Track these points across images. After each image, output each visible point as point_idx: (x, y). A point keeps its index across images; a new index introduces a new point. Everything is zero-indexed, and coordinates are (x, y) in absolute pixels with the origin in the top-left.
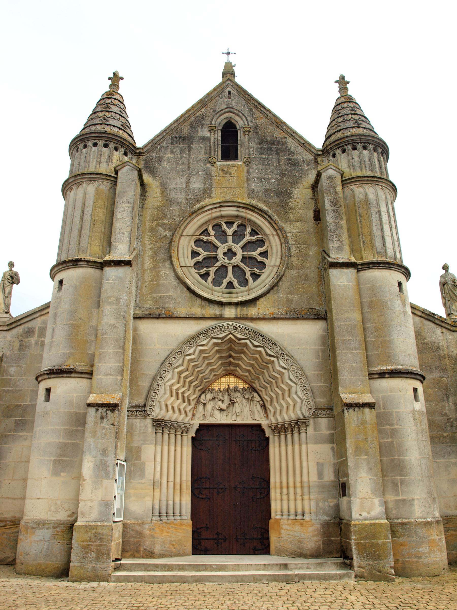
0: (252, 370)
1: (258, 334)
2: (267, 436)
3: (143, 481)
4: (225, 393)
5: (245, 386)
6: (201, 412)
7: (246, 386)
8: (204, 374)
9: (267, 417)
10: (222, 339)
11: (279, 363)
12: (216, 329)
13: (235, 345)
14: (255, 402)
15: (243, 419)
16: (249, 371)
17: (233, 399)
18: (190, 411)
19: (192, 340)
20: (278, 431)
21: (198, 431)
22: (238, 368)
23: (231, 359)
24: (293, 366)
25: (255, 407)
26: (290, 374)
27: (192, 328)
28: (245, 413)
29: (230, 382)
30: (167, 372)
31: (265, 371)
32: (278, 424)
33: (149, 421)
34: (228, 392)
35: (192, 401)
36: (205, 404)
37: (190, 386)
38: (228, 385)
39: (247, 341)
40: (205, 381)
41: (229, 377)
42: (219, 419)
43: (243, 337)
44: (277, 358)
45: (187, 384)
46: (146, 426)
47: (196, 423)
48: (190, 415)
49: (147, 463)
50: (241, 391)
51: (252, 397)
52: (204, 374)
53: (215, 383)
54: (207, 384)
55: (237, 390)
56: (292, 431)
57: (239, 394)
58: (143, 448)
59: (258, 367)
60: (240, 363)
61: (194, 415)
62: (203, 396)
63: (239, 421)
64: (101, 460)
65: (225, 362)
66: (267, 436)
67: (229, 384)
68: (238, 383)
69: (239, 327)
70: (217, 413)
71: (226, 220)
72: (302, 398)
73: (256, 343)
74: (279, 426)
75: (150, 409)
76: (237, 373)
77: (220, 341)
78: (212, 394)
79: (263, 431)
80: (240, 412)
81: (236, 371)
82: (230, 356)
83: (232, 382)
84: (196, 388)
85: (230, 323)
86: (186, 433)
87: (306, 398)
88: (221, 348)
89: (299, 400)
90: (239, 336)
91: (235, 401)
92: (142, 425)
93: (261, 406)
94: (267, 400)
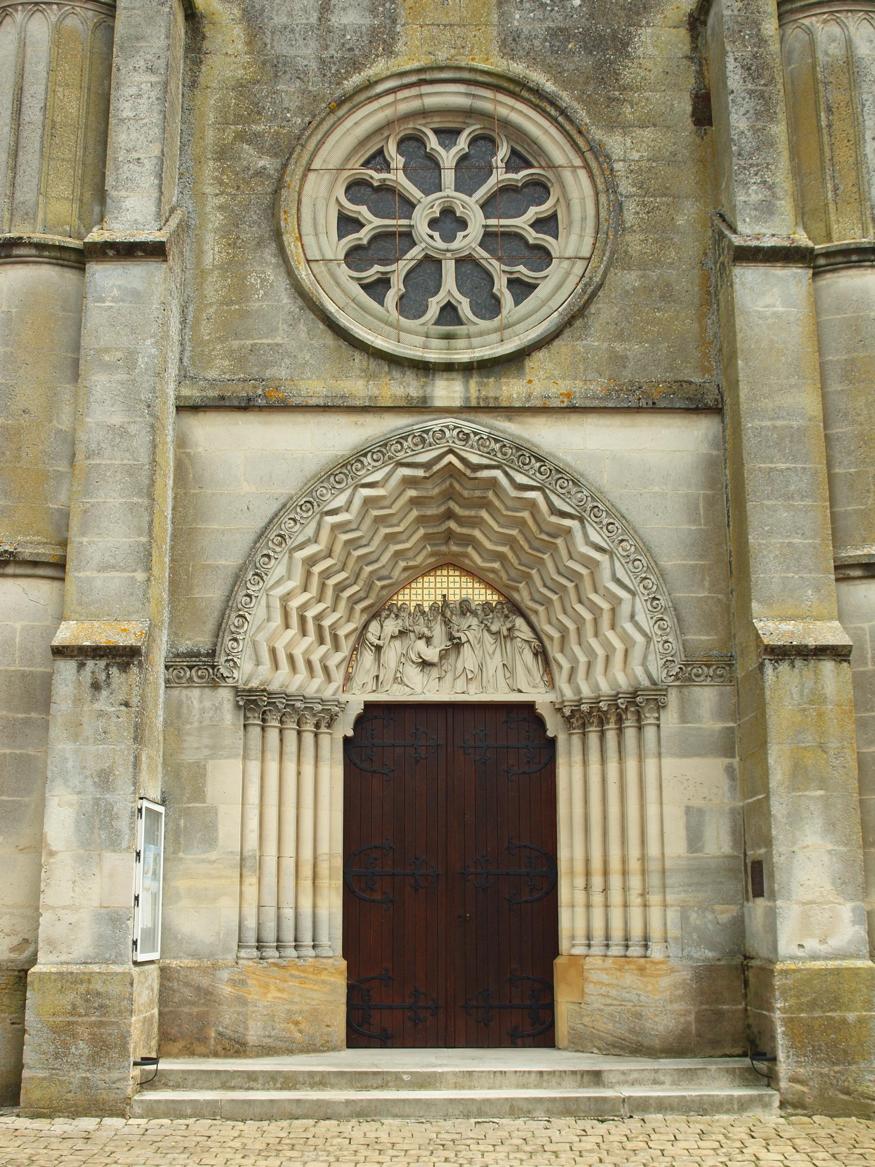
0: (510, 555)
1: (526, 454)
2: (550, 734)
3: (213, 855)
4: (435, 618)
5: (489, 598)
6: (368, 671)
7: (493, 598)
8: (375, 566)
9: (551, 684)
10: (427, 466)
11: (586, 535)
12: (410, 439)
13: (461, 485)
14: (518, 643)
15: (483, 689)
16: (500, 557)
17: (457, 635)
18: (338, 666)
19: (343, 470)
20: (580, 722)
21: (360, 721)
22: (470, 550)
23: (452, 525)
24: (624, 544)
25: (518, 657)
26: (617, 564)
27: (342, 435)
28: (491, 672)
29: (448, 588)
30: (273, 561)
31: (545, 557)
32: (580, 702)
33: (225, 695)
34: (443, 615)
35: (342, 640)
36: (379, 648)
37: (337, 599)
38: (444, 596)
39: (498, 474)
40: (379, 584)
41: (445, 572)
42: (418, 689)
43: (485, 461)
44: (581, 520)
45: (329, 592)
46: (217, 709)
47: (356, 701)
48: (338, 677)
49: (222, 809)
50: (479, 612)
51: (509, 630)
52: (375, 566)
53: (407, 591)
54: (384, 592)
55: (468, 610)
56: (620, 720)
57: (474, 622)
58: (209, 767)
59: (526, 547)
60: (477, 533)
61: (348, 678)
62: (374, 627)
63: (474, 695)
64: (97, 802)
65: (435, 530)
66: (550, 734)
67: (445, 592)
68: (470, 591)
69: (476, 434)
70: (413, 673)
71: (438, 122)
72: (648, 631)
73: (521, 479)
74: (585, 708)
75: (227, 661)
76: (467, 561)
77: (420, 473)
78: (400, 621)
79: (540, 722)
80: (476, 670)
81: (466, 555)
82: (450, 515)
83: (454, 587)
84: (356, 603)
85: (450, 421)
86: (329, 726)
87: (659, 632)
88: (424, 494)
89: (639, 638)
90: (474, 459)
91: (464, 639)
92: (207, 704)
93: (536, 655)
94: (551, 638)
